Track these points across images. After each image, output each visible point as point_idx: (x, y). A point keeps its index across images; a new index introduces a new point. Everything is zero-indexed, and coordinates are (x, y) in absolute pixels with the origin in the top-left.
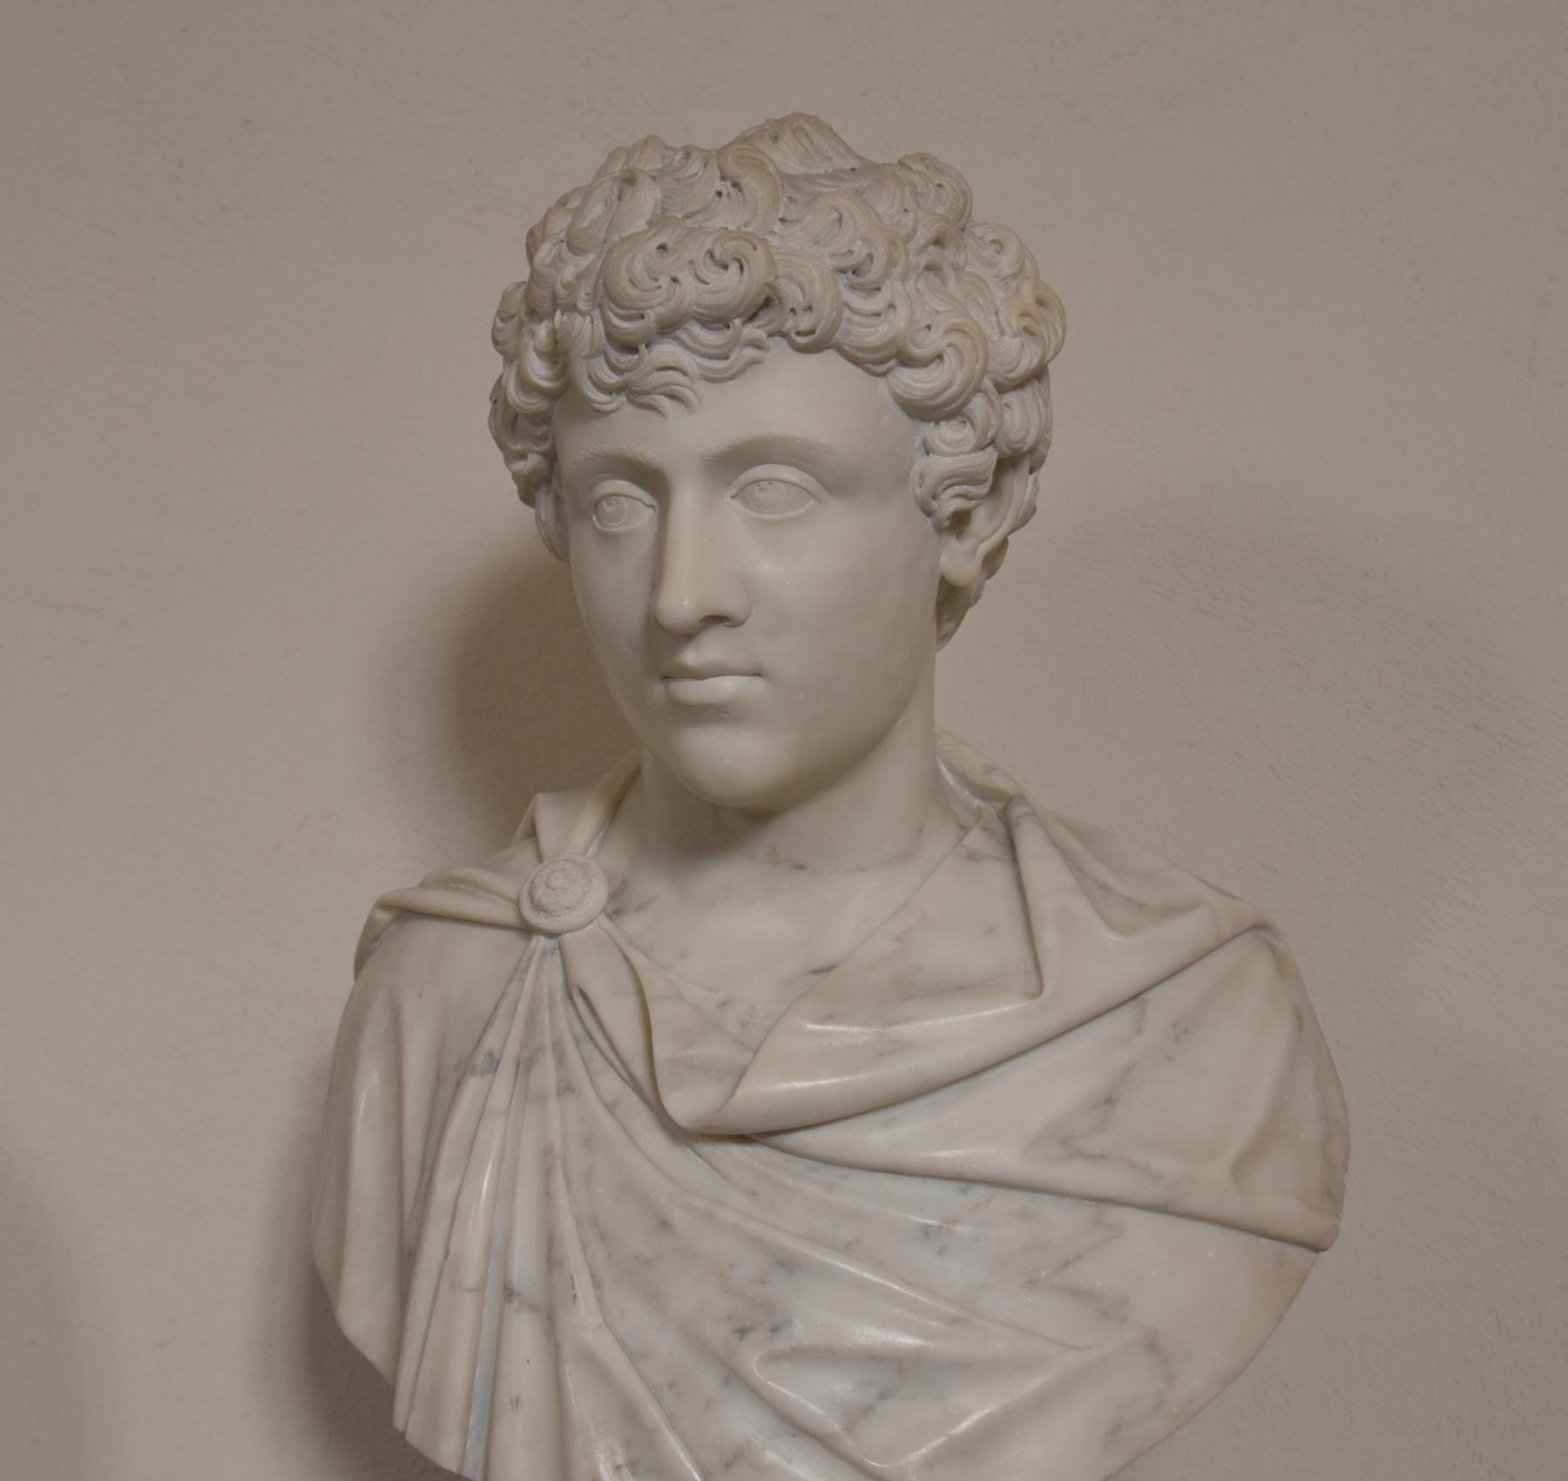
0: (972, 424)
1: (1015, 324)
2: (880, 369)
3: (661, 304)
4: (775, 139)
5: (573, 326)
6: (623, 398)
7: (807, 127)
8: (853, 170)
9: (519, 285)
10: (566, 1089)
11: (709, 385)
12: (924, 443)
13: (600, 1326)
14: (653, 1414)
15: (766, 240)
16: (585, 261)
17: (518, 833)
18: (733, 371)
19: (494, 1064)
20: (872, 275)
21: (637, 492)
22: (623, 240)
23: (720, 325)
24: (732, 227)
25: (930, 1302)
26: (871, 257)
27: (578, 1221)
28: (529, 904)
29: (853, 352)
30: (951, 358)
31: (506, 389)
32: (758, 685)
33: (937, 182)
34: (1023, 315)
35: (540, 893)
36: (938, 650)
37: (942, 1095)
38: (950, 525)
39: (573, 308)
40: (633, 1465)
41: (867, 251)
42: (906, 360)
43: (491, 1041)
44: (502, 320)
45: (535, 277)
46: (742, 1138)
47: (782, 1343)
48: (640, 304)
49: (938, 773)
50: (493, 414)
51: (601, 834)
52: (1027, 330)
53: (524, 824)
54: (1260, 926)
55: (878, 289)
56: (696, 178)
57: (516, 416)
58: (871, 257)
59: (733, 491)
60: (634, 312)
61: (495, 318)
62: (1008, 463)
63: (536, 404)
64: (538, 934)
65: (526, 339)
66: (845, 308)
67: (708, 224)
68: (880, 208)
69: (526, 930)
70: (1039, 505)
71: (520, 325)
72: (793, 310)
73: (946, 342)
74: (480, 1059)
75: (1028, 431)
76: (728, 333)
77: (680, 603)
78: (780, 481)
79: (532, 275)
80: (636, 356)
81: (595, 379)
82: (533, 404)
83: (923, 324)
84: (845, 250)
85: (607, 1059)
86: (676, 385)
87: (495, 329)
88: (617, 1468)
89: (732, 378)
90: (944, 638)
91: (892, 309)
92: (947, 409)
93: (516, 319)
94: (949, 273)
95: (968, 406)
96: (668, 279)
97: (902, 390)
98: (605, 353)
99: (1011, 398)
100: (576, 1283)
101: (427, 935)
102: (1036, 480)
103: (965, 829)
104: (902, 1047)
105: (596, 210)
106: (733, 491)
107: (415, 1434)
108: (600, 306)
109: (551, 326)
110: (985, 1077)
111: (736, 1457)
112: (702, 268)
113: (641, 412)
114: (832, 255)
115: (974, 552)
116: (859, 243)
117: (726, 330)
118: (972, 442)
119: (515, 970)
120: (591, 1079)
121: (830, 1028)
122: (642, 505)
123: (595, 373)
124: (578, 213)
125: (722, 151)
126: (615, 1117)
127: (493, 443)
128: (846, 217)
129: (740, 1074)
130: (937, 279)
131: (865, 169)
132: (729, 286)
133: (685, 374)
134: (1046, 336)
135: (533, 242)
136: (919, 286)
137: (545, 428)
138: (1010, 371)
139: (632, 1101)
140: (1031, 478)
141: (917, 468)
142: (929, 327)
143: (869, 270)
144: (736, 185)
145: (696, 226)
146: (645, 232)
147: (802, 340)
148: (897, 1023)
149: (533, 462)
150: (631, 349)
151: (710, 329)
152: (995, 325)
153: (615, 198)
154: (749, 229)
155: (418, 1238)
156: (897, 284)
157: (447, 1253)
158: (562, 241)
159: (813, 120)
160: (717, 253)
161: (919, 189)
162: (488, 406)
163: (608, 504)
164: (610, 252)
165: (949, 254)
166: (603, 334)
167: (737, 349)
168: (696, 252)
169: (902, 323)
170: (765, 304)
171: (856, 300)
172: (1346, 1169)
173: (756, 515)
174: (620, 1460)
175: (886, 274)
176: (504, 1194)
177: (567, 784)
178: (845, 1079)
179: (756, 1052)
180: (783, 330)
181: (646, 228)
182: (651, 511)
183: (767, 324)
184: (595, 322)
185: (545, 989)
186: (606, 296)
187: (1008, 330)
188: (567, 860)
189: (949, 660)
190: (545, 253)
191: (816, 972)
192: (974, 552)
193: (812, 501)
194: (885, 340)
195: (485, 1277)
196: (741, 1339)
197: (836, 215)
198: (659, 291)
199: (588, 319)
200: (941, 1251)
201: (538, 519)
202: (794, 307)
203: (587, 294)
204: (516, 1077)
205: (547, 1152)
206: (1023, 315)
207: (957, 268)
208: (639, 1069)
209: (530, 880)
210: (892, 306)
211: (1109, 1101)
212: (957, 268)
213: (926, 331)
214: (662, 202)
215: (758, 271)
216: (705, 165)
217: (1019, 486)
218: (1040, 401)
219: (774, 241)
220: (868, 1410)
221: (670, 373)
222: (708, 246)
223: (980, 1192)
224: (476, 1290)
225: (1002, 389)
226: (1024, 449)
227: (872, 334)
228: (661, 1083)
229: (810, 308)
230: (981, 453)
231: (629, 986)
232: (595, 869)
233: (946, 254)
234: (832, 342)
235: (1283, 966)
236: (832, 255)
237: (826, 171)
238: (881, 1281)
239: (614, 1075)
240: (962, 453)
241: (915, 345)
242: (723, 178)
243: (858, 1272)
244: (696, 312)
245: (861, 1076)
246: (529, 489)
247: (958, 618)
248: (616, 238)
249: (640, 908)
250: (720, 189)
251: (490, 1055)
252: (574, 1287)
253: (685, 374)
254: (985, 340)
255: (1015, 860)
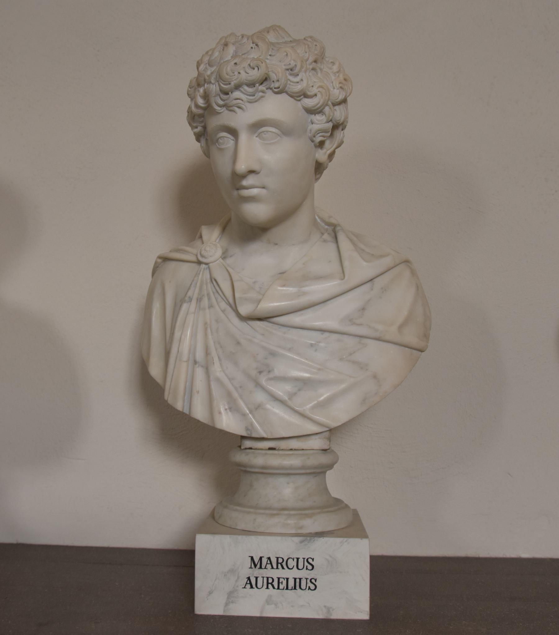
0: (325, 115)
1: (338, 85)
2: (299, 99)
3: (235, 80)
4: (268, 32)
5: (210, 88)
6: (225, 108)
7: (277, 28)
8: (291, 41)
9: (195, 78)
10: (211, 306)
11: (249, 104)
12: (311, 121)
13: (221, 371)
14: (236, 395)
15: (266, 61)
16: (213, 69)
17: (197, 237)
18: (256, 99)
19: (191, 300)
20: (296, 71)
21: (229, 136)
22: (224, 62)
23: (252, 86)
24: (255, 57)
25: (313, 364)
26: (296, 65)
27: (214, 342)
28: (200, 256)
29: (291, 93)
30: (319, 95)
31: (191, 107)
32: (264, 191)
33: (315, 44)
34: (340, 83)
35: (203, 252)
36: (315, 183)
37: (316, 307)
38: (319, 145)
39: (210, 83)
40: (230, 409)
41: (295, 64)
42: (306, 96)
43: (190, 293)
44: (190, 88)
45: (199, 74)
46: (260, 319)
47: (271, 375)
48: (229, 80)
49: (315, 219)
50: (188, 116)
51: (220, 236)
52: (341, 87)
53: (198, 235)
54: (407, 261)
55: (298, 75)
56: (245, 43)
57: (195, 116)
58: (296, 65)
59: (256, 135)
60: (227, 82)
61: (188, 88)
62: (336, 127)
63: (200, 111)
64: (203, 264)
65: (197, 93)
66: (288, 80)
67: (249, 57)
68: (299, 51)
69: (199, 263)
70: (344, 140)
71: (195, 89)
72: (273, 81)
73: (318, 90)
74: (187, 298)
75: (341, 117)
76: (255, 88)
77: (241, 167)
78: (270, 131)
79: (198, 74)
80: (228, 96)
81: (217, 103)
82: (198, 112)
83: (311, 85)
84: (288, 64)
85: (222, 298)
86: (240, 104)
87: (188, 91)
88: (226, 409)
89: (256, 101)
90: (317, 179)
91: (302, 81)
92: (318, 110)
93: (194, 87)
94: (319, 70)
95: (324, 110)
96: (237, 73)
97: (305, 105)
98: (219, 95)
99: (337, 108)
100: (214, 359)
101: (172, 265)
102: (343, 133)
103: (323, 234)
104: (305, 294)
105: (217, 54)
106: (256, 135)
107: (170, 401)
108: (218, 81)
109: (204, 88)
110: (329, 302)
111: (259, 407)
112: (247, 69)
113: (230, 112)
114: (285, 65)
115: (326, 153)
116: (292, 61)
117: (254, 88)
118: (325, 120)
119: (196, 274)
120: (218, 304)
121: (285, 288)
122: (231, 140)
123: (217, 101)
124: (211, 56)
125: (253, 35)
126: (225, 314)
127: (188, 124)
128: (289, 54)
129: (259, 301)
130: (315, 73)
131: (294, 41)
132: (255, 74)
133: (242, 101)
134: (347, 90)
135: (198, 64)
136: (310, 74)
137: (202, 119)
138: (337, 99)
139: (229, 309)
140: (342, 132)
141: (309, 128)
142: (313, 86)
143: (295, 70)
144: (257, 45)
145: (245, 57)
146: (231, 59)
147: (276, 90)
148: (304, 287)
149: (199, 129)
150: (227, 93)
151: (250, 87)
152: (332, 86)
153: (222, 50)
154: (261, 58)
155: (170, 348)
156: (304, 74)
157: (178, 351)
158: (207, 64)
159: (279, 27)
160: (251, 65)
161: (310, 46)
162: (187, 114)
163: (221, 140)
164: (220, 65)
165: (319, 65)
166: (219, 89)
167: (257, 93)
168: (245, 64)
169: (305, 85)
170: (265, 80)
171: (291, 78)
172: (430, 329)
173: (263, 142)
174: (227, 407)
175: (300, 71)
176: (194, 335)
177: (210, 223)
178: (289, 302)
179: (264, 295)
180: (271, 87)
181: (230, 58)
182: (233, 141)
183: (266, 86)
184: (216, 86)
185: (205, 279)
186: (220, 78)
187: (336, 88)
188: (210, 243)
189: (318, 186)
190: (202, 67)
191: (280, 273)
192: (326, 153)
193: (279, 138)
194: (300, 90)
195: (189, 357)
196: (260, 374)
197: (286, 53)
198: (235, 76)
199: (214, 85)
200: (316, 350)
201: (201, 145)
202: (274, 80)
203: (214, 78)
204: (197, 303)
205: (206, 324)
206: (340, 83)
207: (321, 69)
208: (231, 300)
209: (200, 249)
210: (302, 80)
211: (363, 309)
212: (321, 69)
213: (312, 87)
214: (235, 51)
215: (263, 70)
216: (248, 39)
217: (339, 134)
218: (345, 109)
219: (268, 61)
220: (295, 394)
221: (238, 100)
222: (249, 63)
223: (326, 334)
224: (186, 362)
225: (334, 105)
226: (340, 123)
227: (297, 88)
228: (237, 306)
229: (278, 81)
230: (328, 124)
231: (228, 278)
232: (218, 245)
233: (318, 65)
234: (284, 91)
235: (413, 273)
236: (285, 65)
237: (283, 41)
238: (299, 358)
239: (224, 302)
240: (322, 124)
241: (309, 91)
242: (253, 43)
243: (292, 356)
244: (246, 82)
245: (293, 302)
246: (198, 137)
247: (321, 173)
248: (222, 61)
249: (231, 256)
250: (252, 47)
251: (190, 297)
252: (213, 360)
253: (242, 101)
254: (329, 90)
255: (337, 242)
